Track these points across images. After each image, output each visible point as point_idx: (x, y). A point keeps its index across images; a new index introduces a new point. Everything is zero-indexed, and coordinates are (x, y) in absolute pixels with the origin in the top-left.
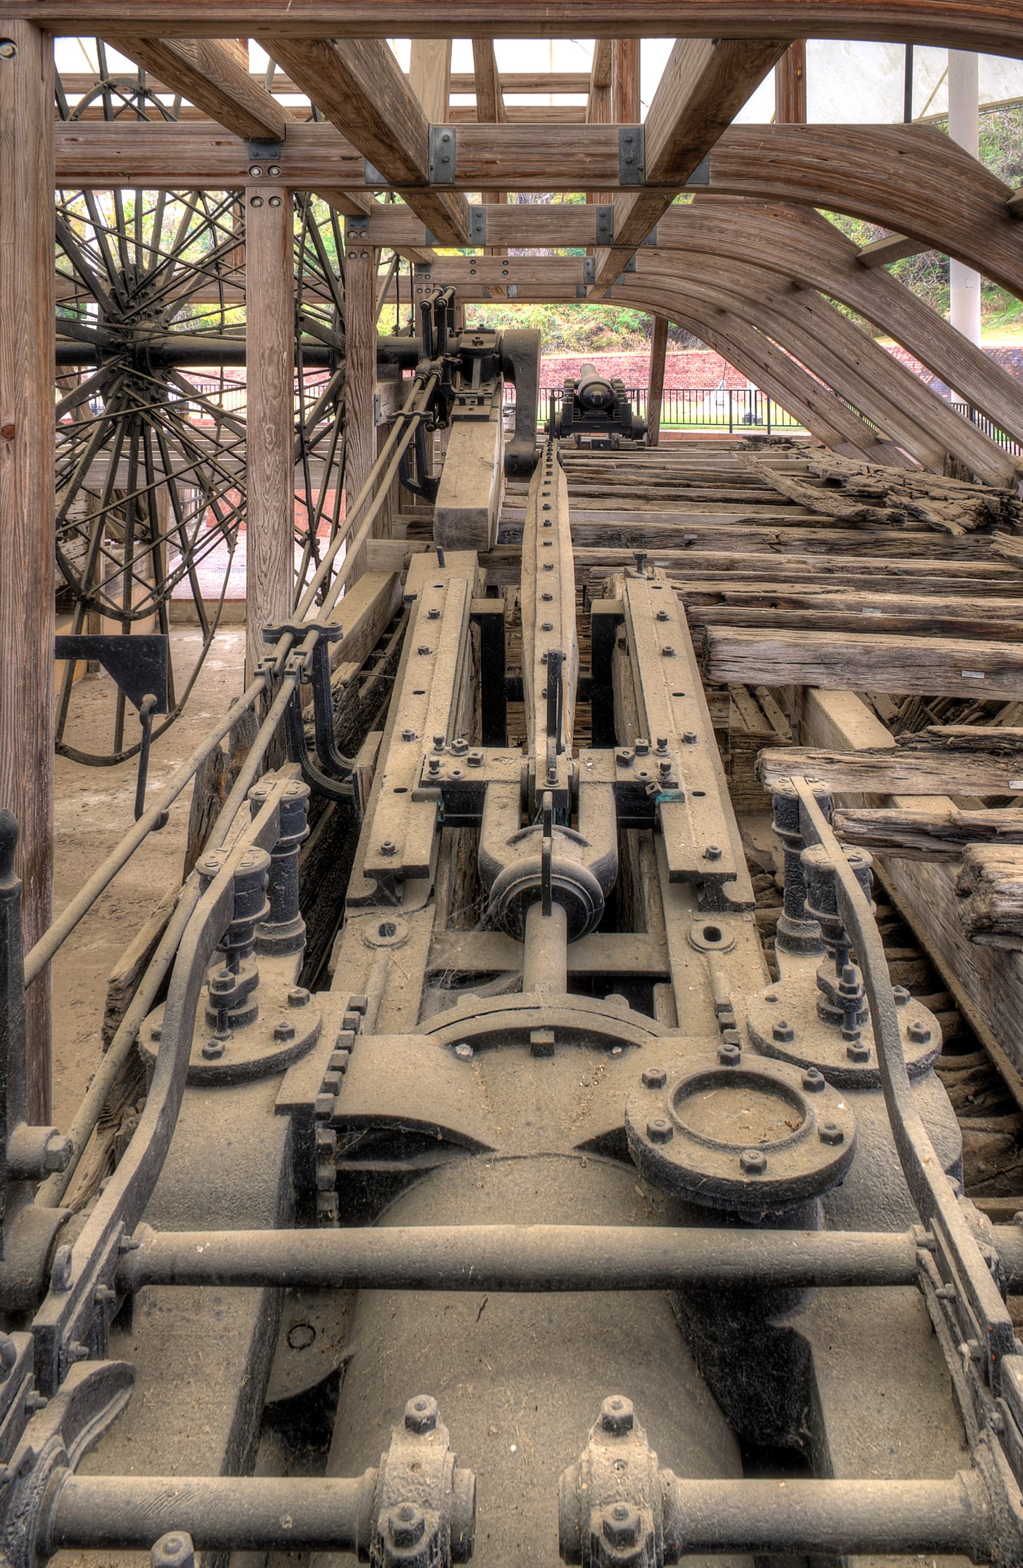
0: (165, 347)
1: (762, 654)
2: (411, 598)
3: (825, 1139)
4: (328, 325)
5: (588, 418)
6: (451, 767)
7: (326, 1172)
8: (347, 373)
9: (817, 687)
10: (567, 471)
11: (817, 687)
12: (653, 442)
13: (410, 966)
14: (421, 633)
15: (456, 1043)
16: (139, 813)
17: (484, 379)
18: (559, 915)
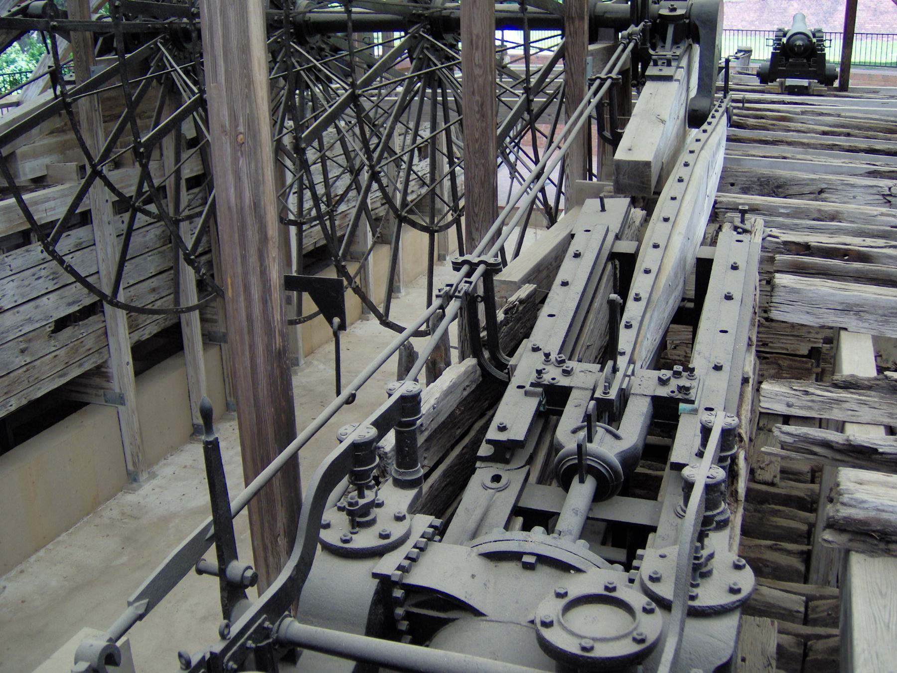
0: (452, 16)
1: (809, 299)
3: (635, 640)
5: (792, 65)
7: (400, 611)
9: (846, 329)
10: (732, 124)
11: (846, 329)
12: (844, 87)
13: (505, 502)
16: (338, 393)
17: (676, 42)
18: (590, 484)
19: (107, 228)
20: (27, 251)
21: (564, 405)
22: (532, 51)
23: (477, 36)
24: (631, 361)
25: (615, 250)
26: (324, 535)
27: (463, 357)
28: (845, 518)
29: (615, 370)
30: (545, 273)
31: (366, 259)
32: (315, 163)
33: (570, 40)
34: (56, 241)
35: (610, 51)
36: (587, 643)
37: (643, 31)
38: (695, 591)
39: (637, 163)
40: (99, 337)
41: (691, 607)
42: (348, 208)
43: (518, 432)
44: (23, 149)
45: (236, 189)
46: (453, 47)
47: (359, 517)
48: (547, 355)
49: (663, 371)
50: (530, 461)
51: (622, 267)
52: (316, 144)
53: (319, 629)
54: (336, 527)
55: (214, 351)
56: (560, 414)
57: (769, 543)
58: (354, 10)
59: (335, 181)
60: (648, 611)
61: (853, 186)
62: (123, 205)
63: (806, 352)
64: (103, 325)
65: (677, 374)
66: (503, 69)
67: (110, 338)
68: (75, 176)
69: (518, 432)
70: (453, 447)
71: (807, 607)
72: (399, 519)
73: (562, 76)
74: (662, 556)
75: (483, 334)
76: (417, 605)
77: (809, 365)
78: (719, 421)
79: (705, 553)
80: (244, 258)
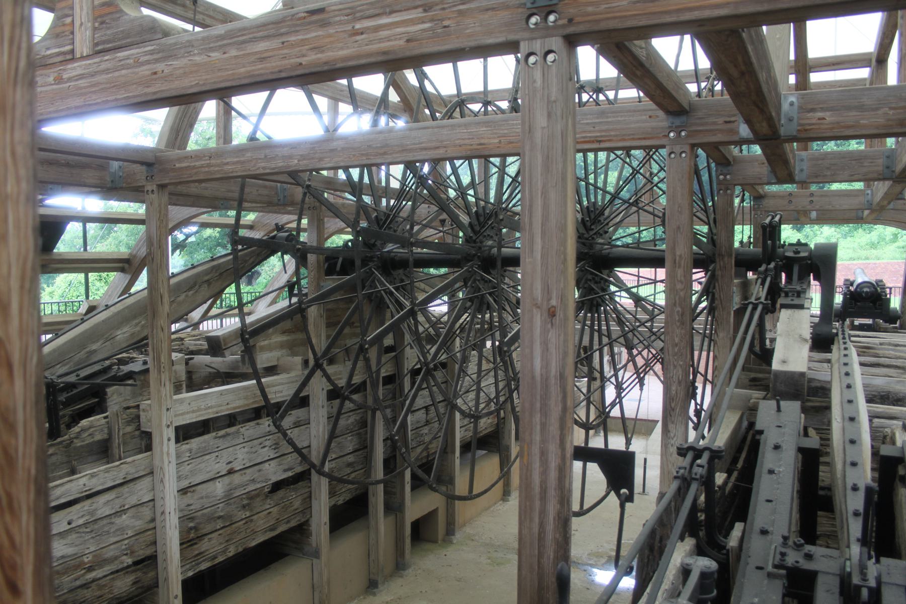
2: (761, 432)
4: (705, 240)
6: (793, 558)
8: (717, 273)
14: (767, 459)
19: (319, 413)
20: (258, 424)
34: (282, 417)
39: (792, 374)
40: (305, 499)
44: (262, 343)
45: (542, 360)
55: (391, 518)
62: (334, 394)
64: (307, 490)
67: (313, 501)
68: (300, 367)
80: (544, 426)
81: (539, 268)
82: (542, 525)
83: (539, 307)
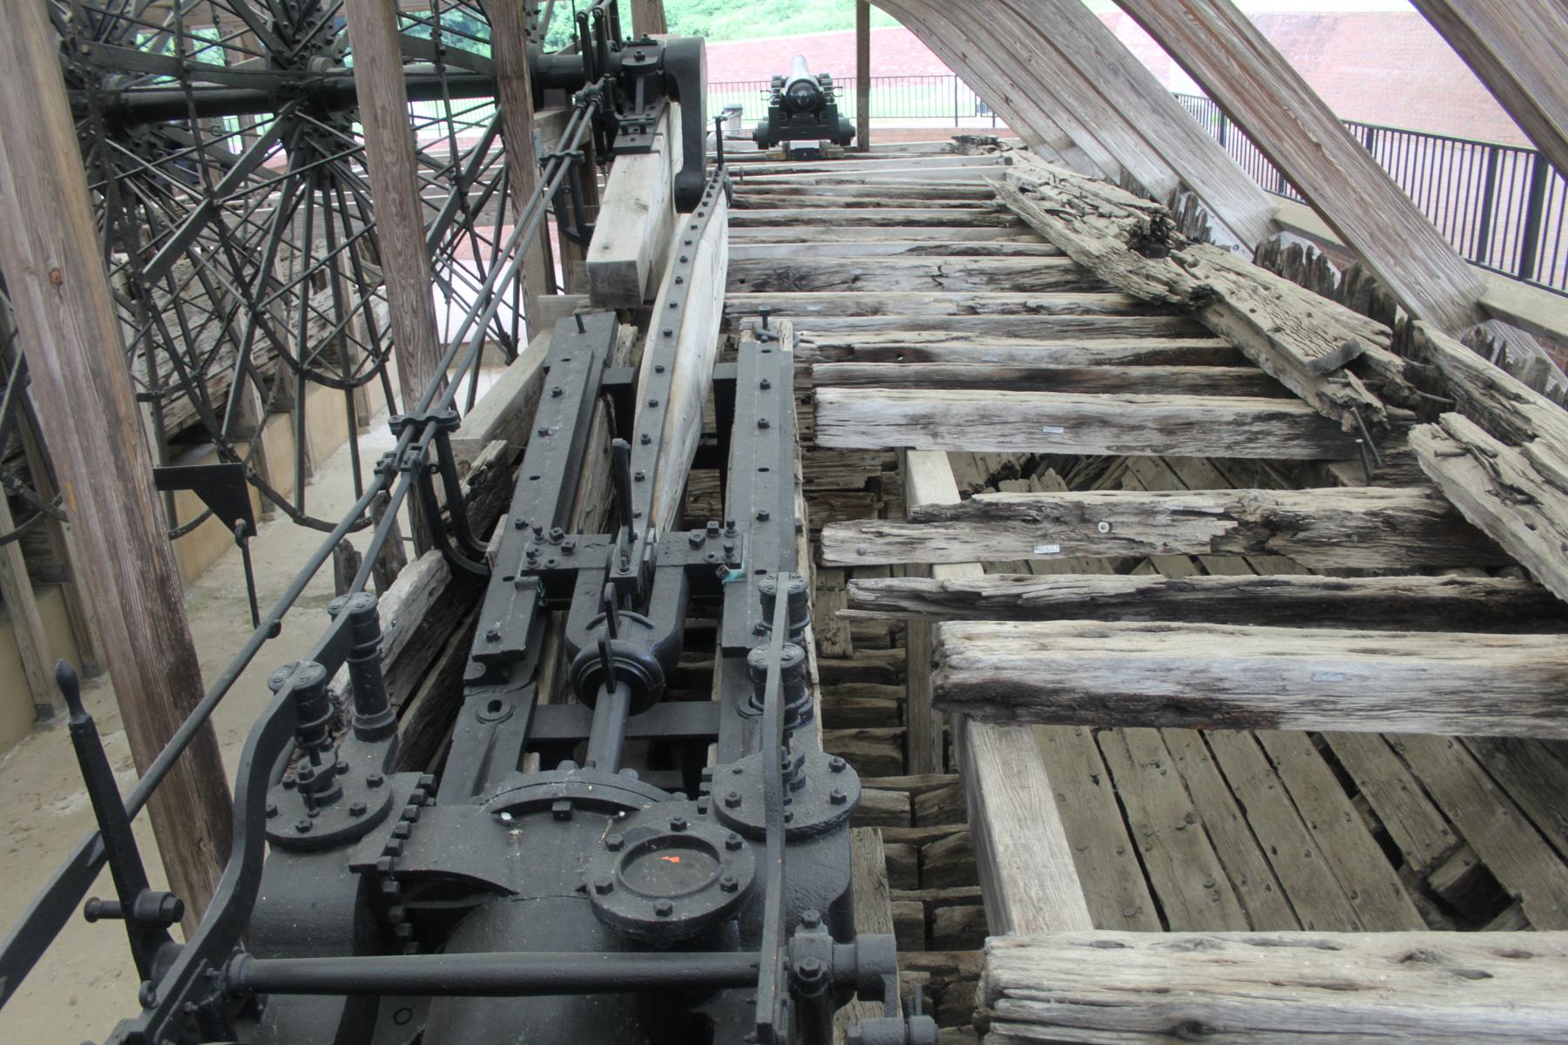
1: (861, 416)
3: (723, 888)
7: (397, 911)
9: (913, 448)
10: (733, 204)
11: (913, 448)
12: (864, 146)
13: (512, 733)
15: (499, 812)
17: (649, 101)
21: (571, 595)
22: (457, 127)
23: (383, 108)
24: (651, 524)
25: (606, 382)
26: (272, 827)
27: (421, 551)
28: (956, 685)
29: (632, 538)
30: (517, 423)
31: (259, 436)
32: (165, 310)
33: (507, 108)
35: (563, 120)
36: (662, 904)
37: (604, 89)
38: (789, 809)
39: (618, 264)
41: (788, 832)
42: (223, 371)
43: (515, 640)
45: (59, 354)
46: (346, 129)
47: (318, 792)
48: (538, 531)
49: (695, 532)
50: (537, 674)
51: (619, 402)
52: (163, 283)
53: (278, 961)
54: (287, 814)
55: (51, 597)
56: (567, 606)
57: (854, 731)
58: (195, 84)
59: (199, 333)
60: (732, 847)
61: (893, 268)
63: (862, 484)
65: (713, 533)
66: (419, 157)
69: (515, 640)
70: (426, 674)
71: (912, 804)
72: (373, 784)
73: (502, 159)
74: (737, 772)
75: (446, 515)
76: (417, 899)
77: (868, 501)
78: (784, 586)
79: (792, 758)
81: (17, 211)
82: (122, 594)
83: (32, 273)
